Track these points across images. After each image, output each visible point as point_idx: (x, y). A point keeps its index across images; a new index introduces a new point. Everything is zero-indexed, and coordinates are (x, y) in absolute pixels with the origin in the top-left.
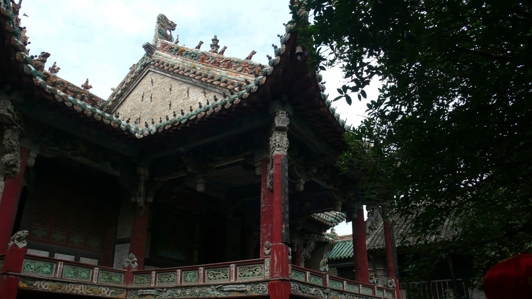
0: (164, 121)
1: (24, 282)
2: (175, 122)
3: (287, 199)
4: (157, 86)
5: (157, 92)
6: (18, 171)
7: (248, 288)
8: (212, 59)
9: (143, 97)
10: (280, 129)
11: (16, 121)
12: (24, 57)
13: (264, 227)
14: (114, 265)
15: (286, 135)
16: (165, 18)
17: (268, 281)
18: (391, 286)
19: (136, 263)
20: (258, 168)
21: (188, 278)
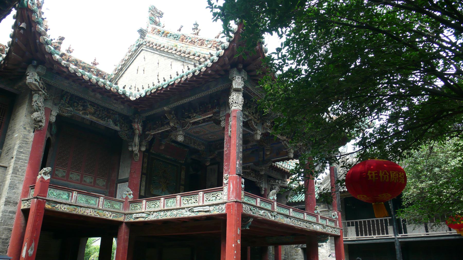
0: (152, 87)
1: (49, 204)
3: (241, 142)
7: (211, 209)
8: (190, 39)
10: (237, 90)
11: (41, 88)
12: (46, 40)
13: (226, 165)
14: (117, 196)
17: (225, 203)
18: (334, 218)
19: (132, 195)
20: (223, 122)
21: (169, 204)
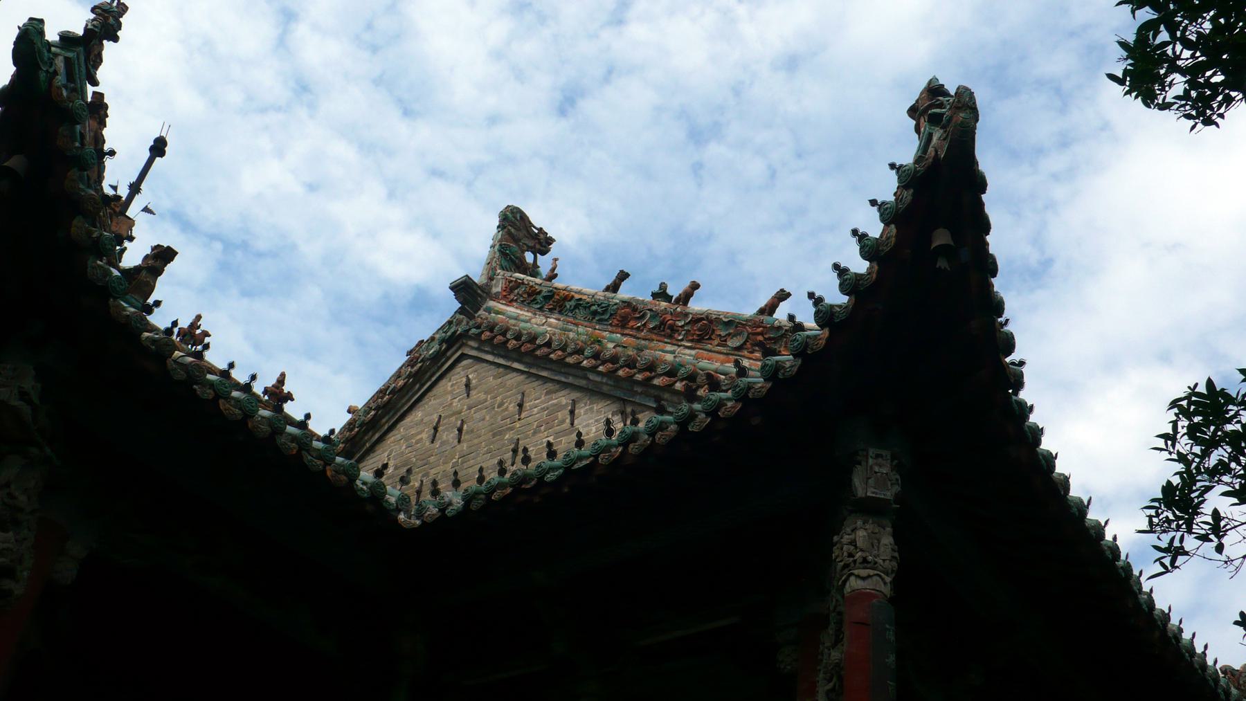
2: (525, 478)
4: (482, 396)
5: (478, 416)
6: (18, 589)
9: (436, 429)
10: (871, 509)
15: (889, 529)
16: (523, 218)
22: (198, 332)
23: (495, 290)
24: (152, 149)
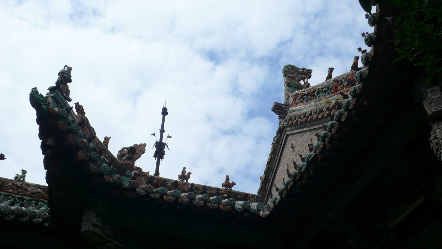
4: (299, 148)
16: (293, 67)
22: (186, 174)
23: (290, 103)
24: (163, 113)
